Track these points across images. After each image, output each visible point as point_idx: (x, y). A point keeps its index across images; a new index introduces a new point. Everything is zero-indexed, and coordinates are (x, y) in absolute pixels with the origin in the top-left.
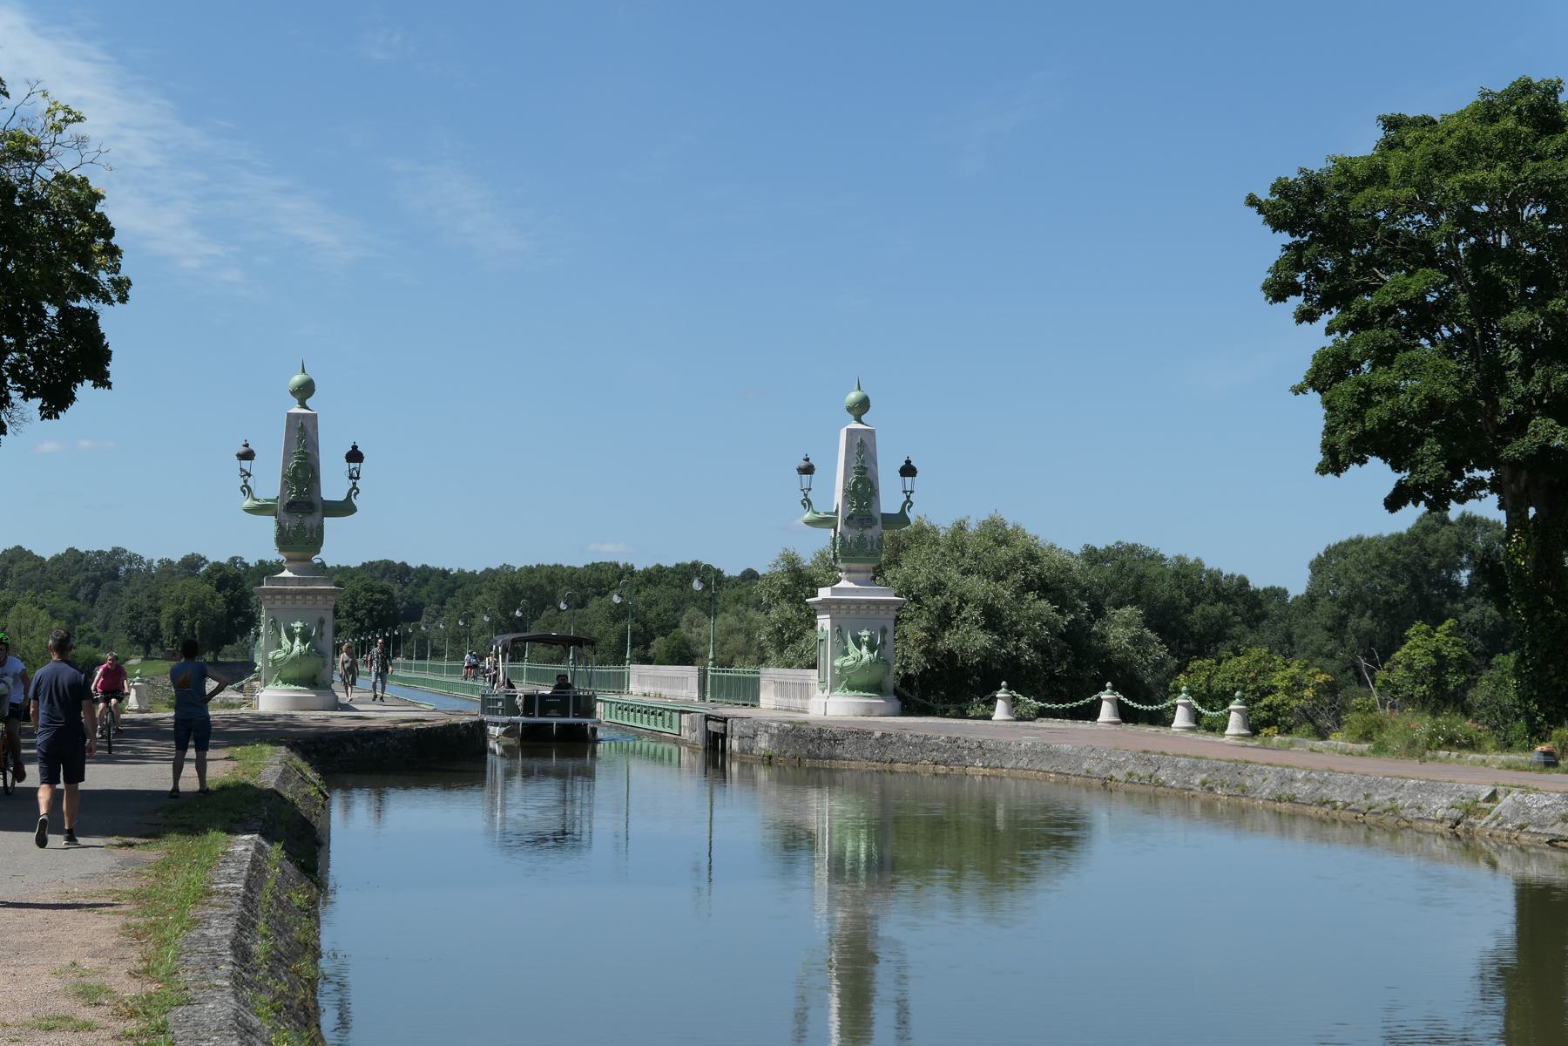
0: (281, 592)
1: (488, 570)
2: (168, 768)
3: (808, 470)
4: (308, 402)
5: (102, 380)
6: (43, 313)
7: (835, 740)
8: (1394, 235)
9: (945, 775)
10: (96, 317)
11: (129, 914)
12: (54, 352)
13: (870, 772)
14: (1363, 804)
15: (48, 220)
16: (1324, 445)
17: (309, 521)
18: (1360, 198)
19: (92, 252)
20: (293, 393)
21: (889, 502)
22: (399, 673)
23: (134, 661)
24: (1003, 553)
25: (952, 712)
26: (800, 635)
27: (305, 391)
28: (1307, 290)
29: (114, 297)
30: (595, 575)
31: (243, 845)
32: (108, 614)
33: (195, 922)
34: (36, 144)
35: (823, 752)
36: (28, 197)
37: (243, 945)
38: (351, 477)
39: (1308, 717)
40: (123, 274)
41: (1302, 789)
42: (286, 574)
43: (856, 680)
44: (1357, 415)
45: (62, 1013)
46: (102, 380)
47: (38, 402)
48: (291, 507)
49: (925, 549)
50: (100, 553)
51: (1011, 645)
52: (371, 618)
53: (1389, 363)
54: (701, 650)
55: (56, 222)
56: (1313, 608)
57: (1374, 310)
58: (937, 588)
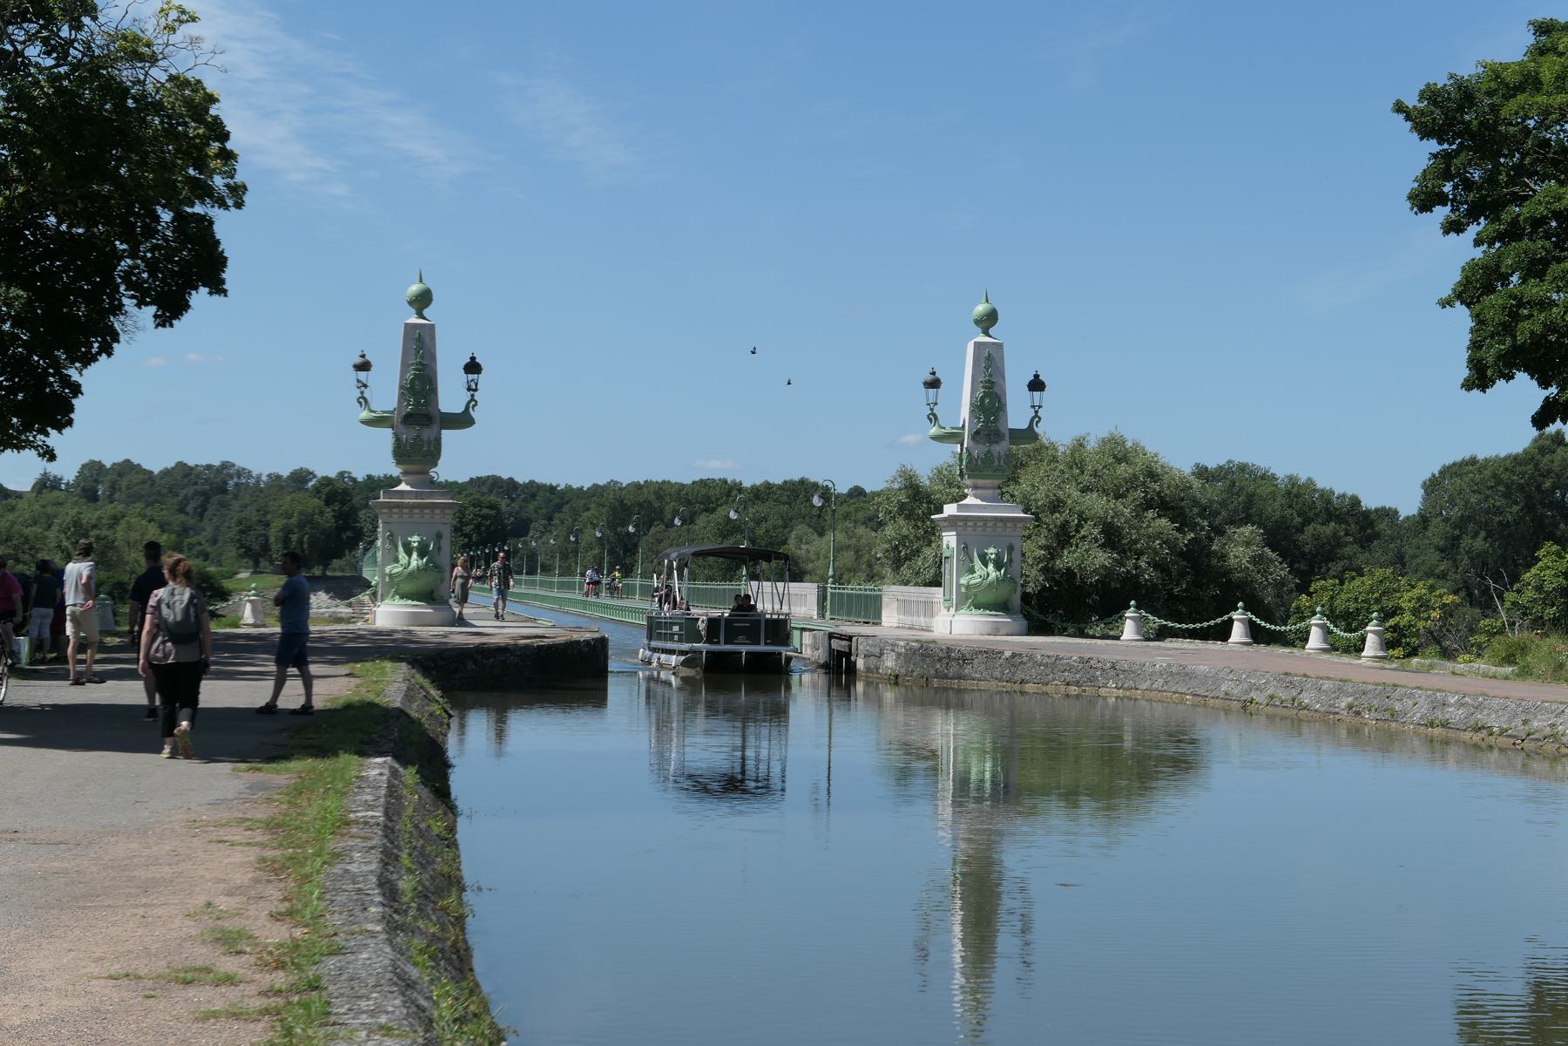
0: (399, 506)
1: (596, 486)
2: (268, 685)
3: (934, 384)
4: (426, 312)
5: (218, 287)
6: (157, 219)
7: (964, 659)
8: (1545, 143)
9: (1077, 696)
10: (211, 223)
11: (262, 845)
12: (169, 259)
13: (1001, 693)
14: (1523, 730)
15: (162, 122)
16: (1471, 360)
17: (427, 434)
18: (1513, 105)
19: (207, 156)
20: (411, 303)
21: (1017, 417)
22: (523, 590)
23: (244, 575)
24: (1123, 470)
25: (1071, 631)
26: (917, 552)
27: (422, 301)
28: (1454, 200)
29: (230, 202)
30: (703, 491)
31: (377, 768)
32: (217, 528)
33: (337, 856)
34: (149, 45)
35: (952, 672)
36: (141, 98)
37: (389, 881)
38: (469, 389)
39: (1435, 638)
40: (239, 178)
41: (1455, 714)
42: (403, 487)
43: (982, 599)
44: (1507, 328)
45: (199, 963)
46: (218, 287)
47: (152, 309)
48: (408, 419)
49: (1044, 467)
50: (209, 467)
51: (1131, 563)
52: (479, 533)
53: (1541, 275)
54: (810, 566)
55: (170, 125)
56: (1425, 528)
57: (1526, 220)
58: (1056, 506)
